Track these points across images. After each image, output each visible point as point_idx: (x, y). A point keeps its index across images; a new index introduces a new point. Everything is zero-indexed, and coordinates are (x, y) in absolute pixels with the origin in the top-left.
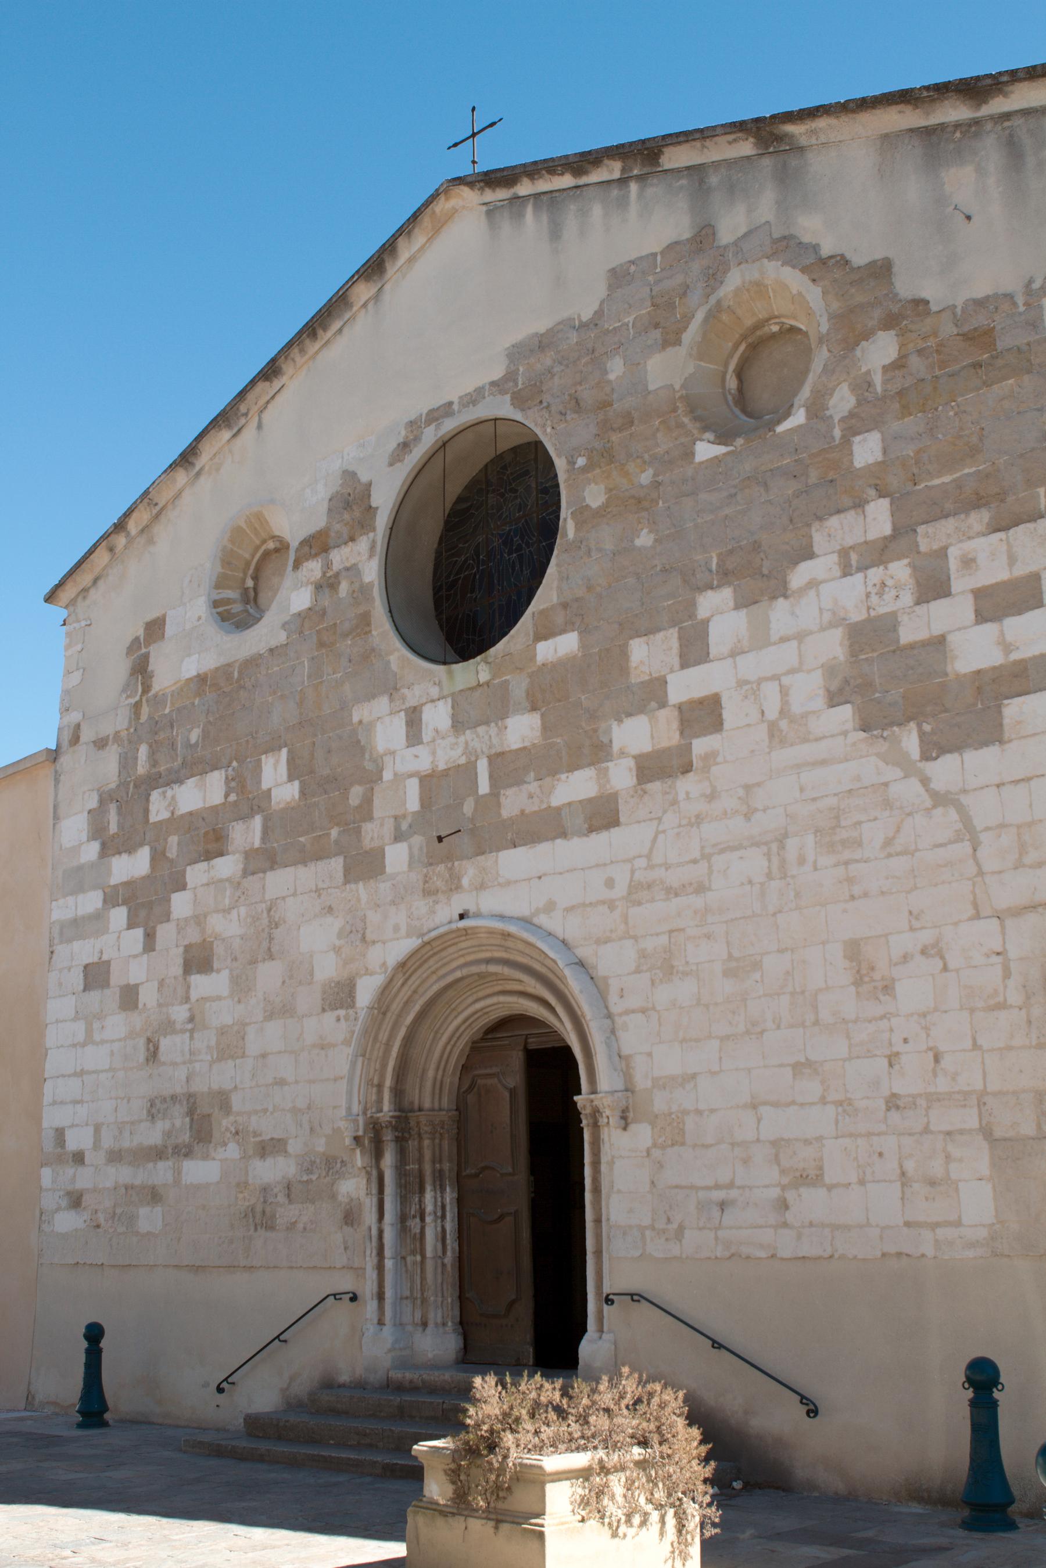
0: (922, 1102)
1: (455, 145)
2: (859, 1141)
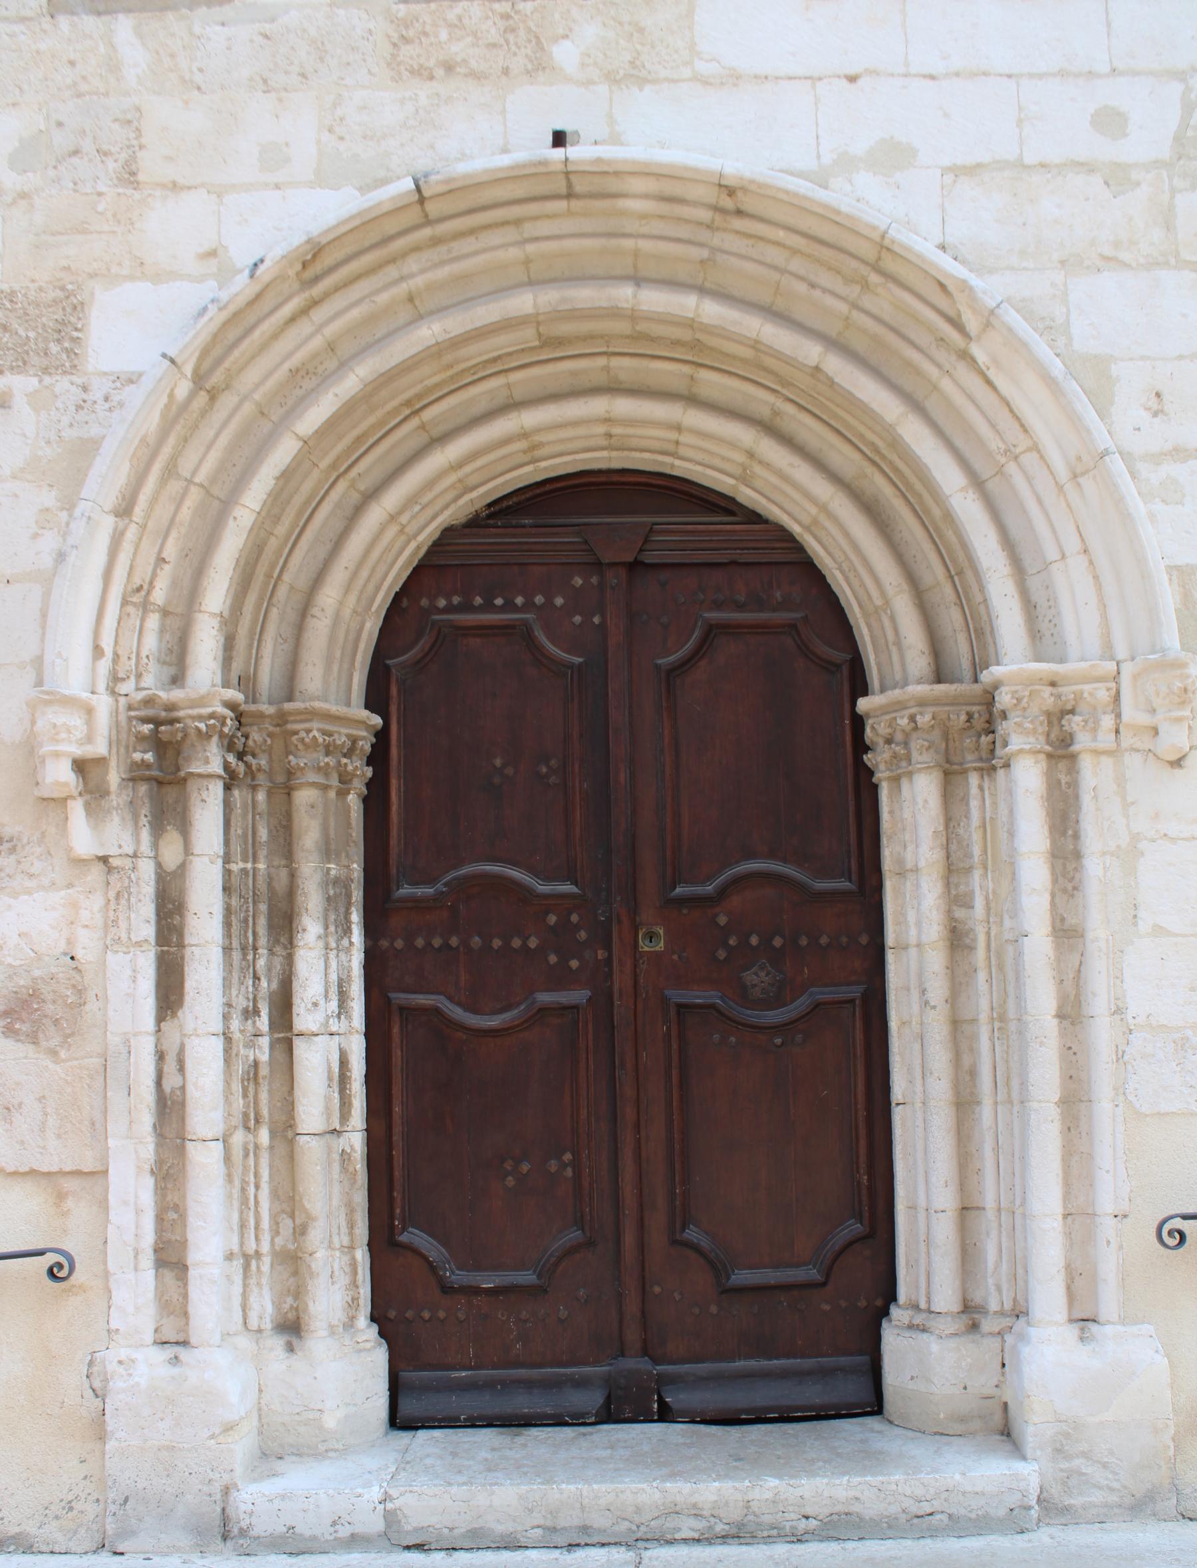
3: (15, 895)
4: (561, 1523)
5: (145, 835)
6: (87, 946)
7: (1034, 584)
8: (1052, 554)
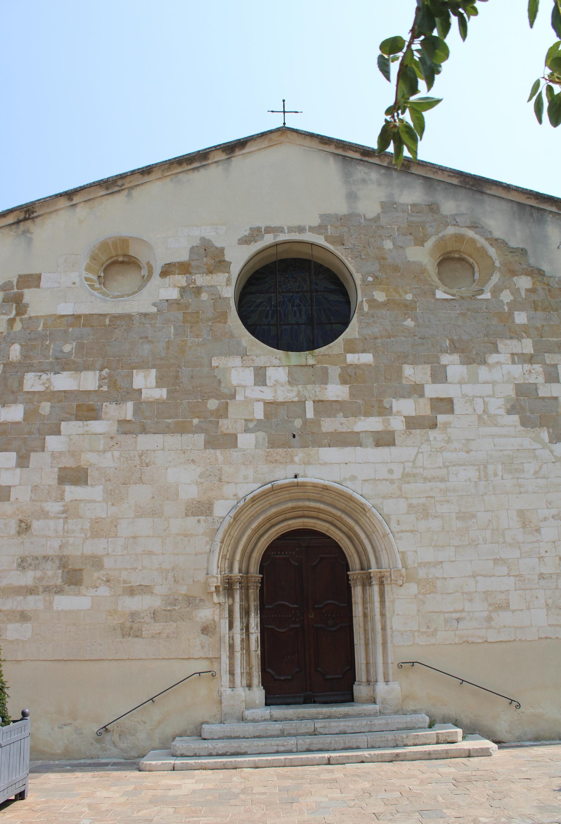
0: (554, 577)
1: (273, 112)
2: (527, 592)
3: (203, 609)
4: (300, 716)
5: (227, 599)
6: (217, 618)
7: (377, 554)
8: (380, 550)
